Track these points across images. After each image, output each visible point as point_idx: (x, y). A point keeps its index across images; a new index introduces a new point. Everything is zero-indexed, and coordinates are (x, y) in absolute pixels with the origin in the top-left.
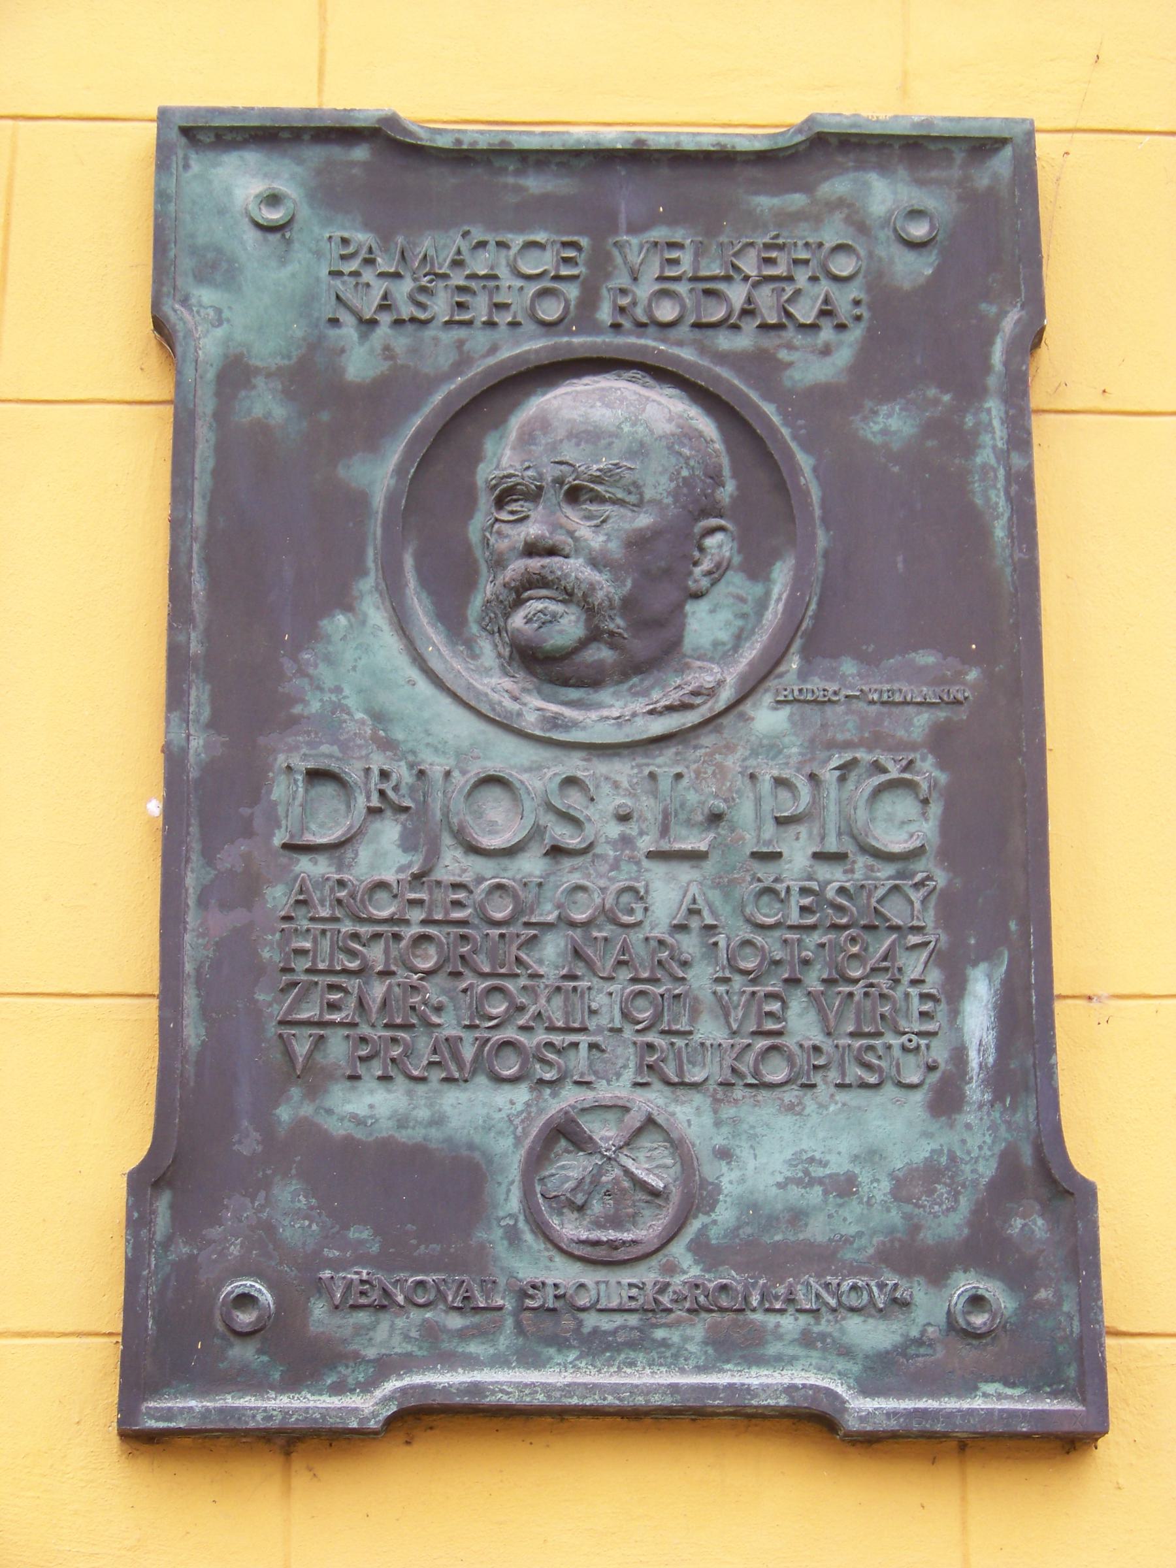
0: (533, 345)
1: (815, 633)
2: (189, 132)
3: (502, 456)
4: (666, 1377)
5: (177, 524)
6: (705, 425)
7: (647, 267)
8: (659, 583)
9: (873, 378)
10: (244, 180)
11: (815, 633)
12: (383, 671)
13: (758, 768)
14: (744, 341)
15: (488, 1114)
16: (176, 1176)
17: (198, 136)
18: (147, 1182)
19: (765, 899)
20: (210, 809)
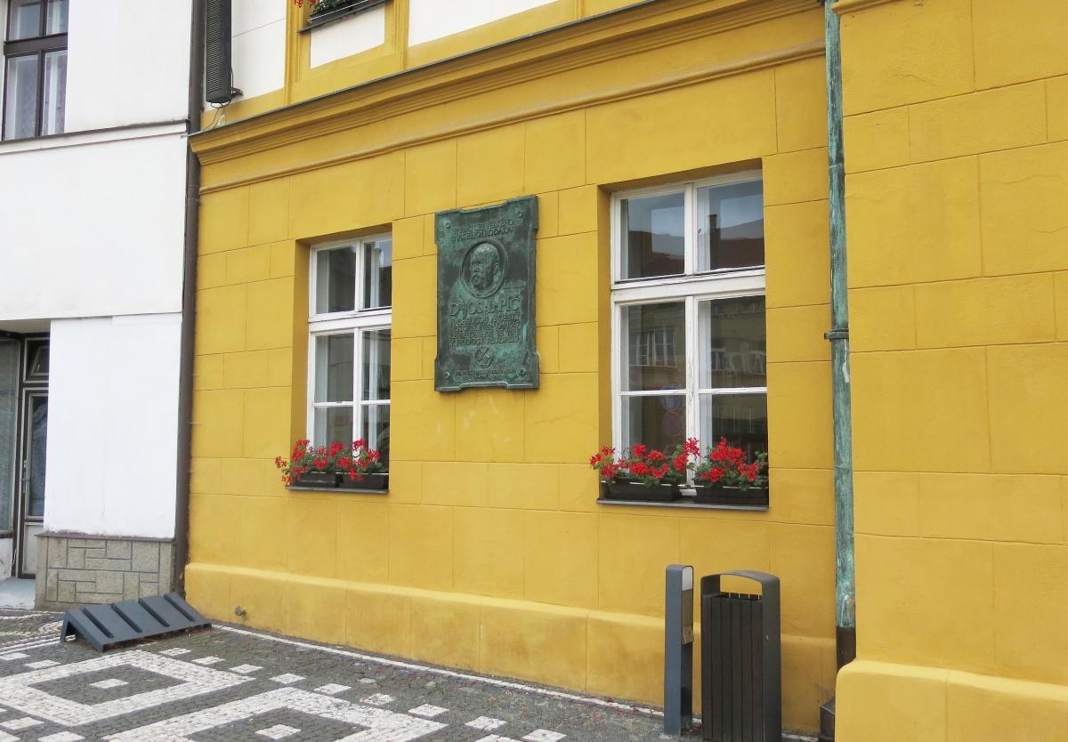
0: (475, 242)
1: (507, 279)
2: (439, 215)
3: (473, 258)
4: (488, 382)
5: (187, 207)
6: (495, 249)
7: (488, 226)
8: (490, 275)
9: (517, 238)
10: (445, 221)
11: (507, 279)
12: (463, 290)
13: (506, 297)
14: (500, 236)
15: (472, 348)
16: (441, 359)
17: (439, 216)
18: (436, 361)
19: (31, 567)
20: (442, 311)
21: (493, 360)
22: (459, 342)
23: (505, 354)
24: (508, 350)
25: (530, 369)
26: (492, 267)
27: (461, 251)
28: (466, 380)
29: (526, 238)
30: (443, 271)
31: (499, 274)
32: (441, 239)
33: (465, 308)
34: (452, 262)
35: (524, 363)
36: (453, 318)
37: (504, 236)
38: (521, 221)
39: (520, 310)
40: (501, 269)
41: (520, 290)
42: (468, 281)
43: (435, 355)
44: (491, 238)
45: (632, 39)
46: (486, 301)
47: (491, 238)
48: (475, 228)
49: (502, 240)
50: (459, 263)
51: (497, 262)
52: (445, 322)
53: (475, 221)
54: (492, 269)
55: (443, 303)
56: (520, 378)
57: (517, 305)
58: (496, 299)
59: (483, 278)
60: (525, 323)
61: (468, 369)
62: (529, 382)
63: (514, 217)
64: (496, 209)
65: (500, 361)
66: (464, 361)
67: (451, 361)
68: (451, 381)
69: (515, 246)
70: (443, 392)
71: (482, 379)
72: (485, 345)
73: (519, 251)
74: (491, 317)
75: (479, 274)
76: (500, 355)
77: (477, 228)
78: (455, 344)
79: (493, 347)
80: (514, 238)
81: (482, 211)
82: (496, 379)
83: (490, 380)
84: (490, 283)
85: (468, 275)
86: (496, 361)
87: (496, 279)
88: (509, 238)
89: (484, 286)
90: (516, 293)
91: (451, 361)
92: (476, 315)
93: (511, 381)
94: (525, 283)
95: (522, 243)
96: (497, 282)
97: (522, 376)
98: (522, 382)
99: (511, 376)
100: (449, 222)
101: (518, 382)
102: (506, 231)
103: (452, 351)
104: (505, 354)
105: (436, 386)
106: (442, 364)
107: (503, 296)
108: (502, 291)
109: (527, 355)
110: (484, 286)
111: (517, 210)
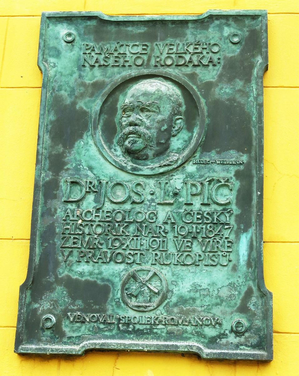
0: (134, 72)
1: (205, 145)
3: (127, 98)
4: (155, 342)
7: (161, 50)
10: (63, 30)
11: (205, 145)
12: (94, 156)
13: (197, 180)
14: (189, 70)
15: (114, 271)
16: (36, 284)
18: (23, 288)
20: (46, 191)
21: (164, 297)
22: (83, 255)
23: (196, 288)
24: (202, 281)
25: (258, 323)
26: (171, 122)
27: (97, 86)
28: (96, 332)
29: (248, 80)
30: (52, 117)
31: (184, 135)
32: (52, 60)
33: (97, 189)
34: (74, 104)
35: (243, 309)
36: (74, 207)
37: (198, 70)
38: (237, 50)
39: (234, 207)
40: (190, 129)
41: (233, 169)
42: (109, 140)
43: (21, 276)
44: (170, 70)
45: (131, 19)
46: (152, 182)
47: (170, 70)
48: (131, 50)
49: (193, 77)
50: (95, 106)
51: (179, 113)
52: (49, 213)
53: (133, 37)
54: (171, 127)
55: (47, 176)
56: (232, 339)
57: (226, 196)
58: (177, 181)
59: (150, 139)
60: (245, 230)
61: (104, 311)
62: (254, 347)
63: (225, 43)
64: (184, 23)
65: (183, 300)
66: (93, 295)
67: (59, 293)
68: (57, 333)
69: (224, 91)
70: (22, 355)
71: (139, 333)
72: (147, 267)
73: (232, 100)
74: (162, 213)
75: (142, 129)
76: (183, 288)
77: (139, 49)
78: (73, 259)
79: (166, 273)
80: (220, 76)
81: (152, 23)
82: (171, 335)
83: (158, 337)
84: (163, 149)
85: (110, 131)
86: (174, 299)
87: (176, 143)
88: (209, 75)
89: (150, 153)
90: (223, 174)
91: (59, 293)
92: (128, 206)
93: (212, 342)
94: (244, 158)
95: (238, 88)
96: (179, 151)
97: (238, 334)
98: (237, 346)
99: (210, 332)
100: (73, 31)
101: (227, 345)
102: (205, 62)
103: (63, 272)
104: (196, 288)
105: (18, 342)
106: (36, 298)
107: (191, 176)
108: (191, 168)
109: (249, 293)
110: (150, 153)
111: (227, 31)
